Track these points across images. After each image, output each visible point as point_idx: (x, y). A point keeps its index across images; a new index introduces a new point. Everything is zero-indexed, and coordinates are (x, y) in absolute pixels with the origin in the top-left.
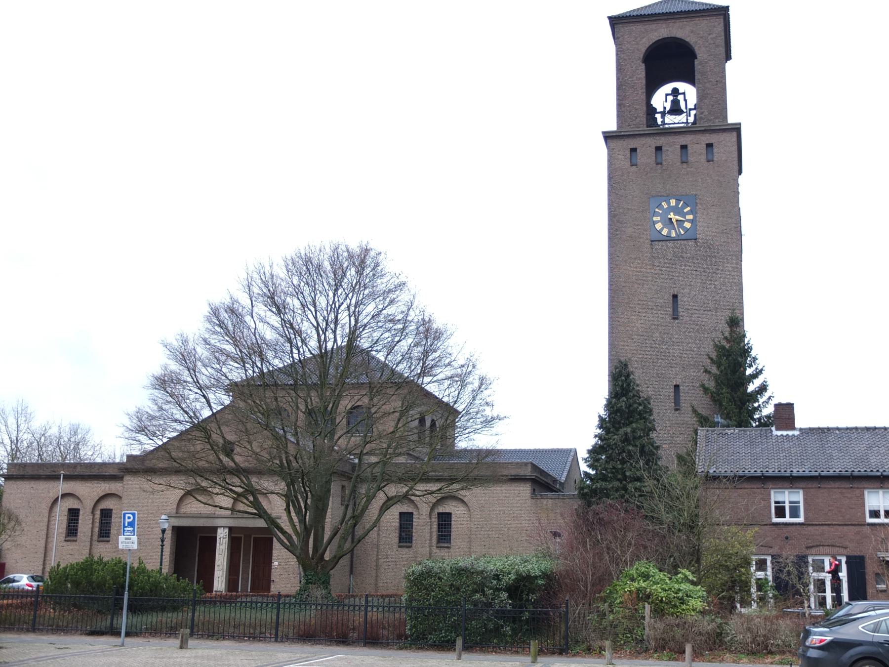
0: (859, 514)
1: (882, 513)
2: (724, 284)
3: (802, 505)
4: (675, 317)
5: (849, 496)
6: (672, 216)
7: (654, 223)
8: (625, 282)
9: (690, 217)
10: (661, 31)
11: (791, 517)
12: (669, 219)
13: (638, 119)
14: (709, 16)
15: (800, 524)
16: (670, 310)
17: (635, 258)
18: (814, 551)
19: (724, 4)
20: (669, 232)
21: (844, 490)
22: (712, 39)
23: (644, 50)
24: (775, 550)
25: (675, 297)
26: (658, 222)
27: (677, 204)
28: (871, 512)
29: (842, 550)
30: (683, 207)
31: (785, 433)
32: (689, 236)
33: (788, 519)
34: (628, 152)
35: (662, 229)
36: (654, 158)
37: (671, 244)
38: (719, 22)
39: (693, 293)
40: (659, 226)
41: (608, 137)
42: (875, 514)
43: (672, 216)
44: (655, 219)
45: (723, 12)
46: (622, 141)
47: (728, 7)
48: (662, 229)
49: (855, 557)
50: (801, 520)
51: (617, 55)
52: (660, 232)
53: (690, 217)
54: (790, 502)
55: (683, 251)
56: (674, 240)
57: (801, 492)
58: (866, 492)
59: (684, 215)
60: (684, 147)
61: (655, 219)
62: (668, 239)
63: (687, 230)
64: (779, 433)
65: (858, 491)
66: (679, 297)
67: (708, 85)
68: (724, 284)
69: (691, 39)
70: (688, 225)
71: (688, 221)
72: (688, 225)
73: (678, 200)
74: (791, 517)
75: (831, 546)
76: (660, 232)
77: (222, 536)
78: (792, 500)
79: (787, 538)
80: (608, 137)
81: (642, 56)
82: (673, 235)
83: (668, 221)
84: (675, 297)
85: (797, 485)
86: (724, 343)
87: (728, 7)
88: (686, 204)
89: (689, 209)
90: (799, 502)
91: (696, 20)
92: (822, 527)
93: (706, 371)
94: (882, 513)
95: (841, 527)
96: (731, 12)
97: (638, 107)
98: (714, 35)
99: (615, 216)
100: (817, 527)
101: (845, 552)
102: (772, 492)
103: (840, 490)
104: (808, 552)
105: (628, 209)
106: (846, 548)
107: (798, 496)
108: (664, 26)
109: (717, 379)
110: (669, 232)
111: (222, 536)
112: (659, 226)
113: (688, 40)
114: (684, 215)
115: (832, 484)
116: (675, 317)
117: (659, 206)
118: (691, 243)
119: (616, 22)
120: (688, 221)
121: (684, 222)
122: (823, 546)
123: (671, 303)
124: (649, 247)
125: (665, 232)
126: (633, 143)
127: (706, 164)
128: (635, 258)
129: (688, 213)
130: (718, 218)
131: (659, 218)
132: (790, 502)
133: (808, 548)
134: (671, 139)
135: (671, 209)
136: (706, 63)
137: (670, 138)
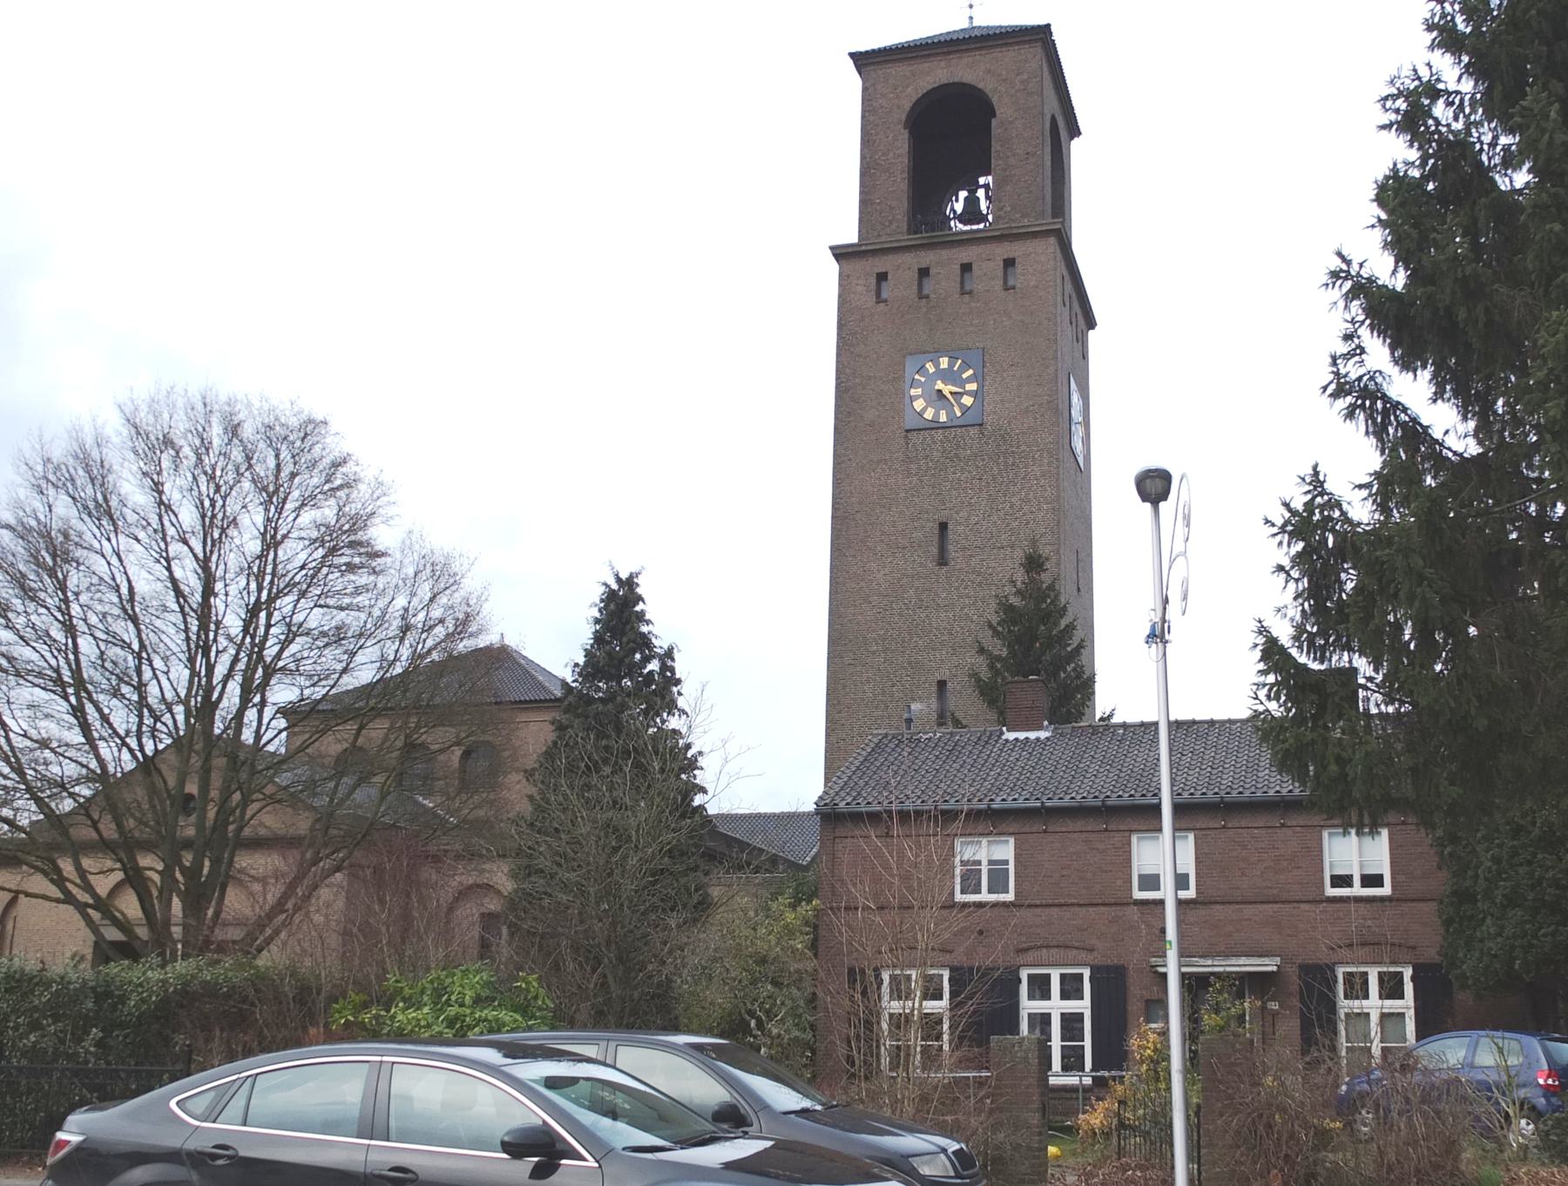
0: (1119, 882)
1: (1357, 881)
2: (1026, 501)
3: (1011, 867)
4: (942, 561)
5: (1101, 846)
6: (940, 385)
7: (912, 399)
8: (860, 503)
9: (972, 387)
10: (939, 73)
11: (990, 891)
12: (936, 392)
13: (894, 226)
14: (1017, 43)
15: (1382, 899)
16: (935, 550)
17: (879, 462)
18: (1030, 956)
19: (1042, 22)
20: (937, 414)
21: (1092, 836)
22: (1022, 82)
23: (907, 106)
24: (959, 958)
25: (943, 527)
26: (918, 397)
27: (951, 365)
28: (1333, 877)
29: (1083, 955)
30: (962, 370)
31: (1022, 735)
32: (969, 420)
33: (985, 896)
34: (873, 281)
35: (924, 409)
36: (915, 287)
37: (939, 435)
38: (1032, 55)
39: (974, 519)
40: (919, 405)
41: (841, 254)
42: (1342, 881)
43: (940, 385)
44: (913, 392)
45: (1041, 36)
46: (863, 262)
47: (1048, 26)
48: (924, 409)
49: (1108, 967)
50: (1010, 897)
51: (863, 117)
52: (920, 414)
53: (972, 387)
54: (991, 862)
55: (958, 446)
56: (944, 427)
57: (1012, 840)
58: (1134, 838)
59: (962, 383)
60: (966, 268)
61: (913, 392)
62: (935, 426)
63: (966, 410)
64: (1011, 736)
65: (1117, 838)
66: (950, 527)
67: (1012, 161)
68: (1026, 501)
69: (987, 85)
70: (967, 401)
71: (968, 393)
72: (967, 401)
73: (953, 359)
74: (990, 891)
75: (1062, 948)
76: (920, 414)
77: (984, 869)
78: (995, 857)
79: (981, 933)
80: (841, 254)
81: (904, 117)
82: (943, 418)
83: (934, 397)
84: (943, 527)
85: (1003, 827)
86: (1015, 601)
87: (1048, 26)
88: (967, 365)
89: (971, 372)
90: (1006, 862)
91: (996, 53)
92: (1047, 910)
93: (982, 651)
94: (1357, 881)
95: (1084, 909)
96: (1058, 36)
97: (895, 204)
98: (1025, 76)
99: (847, 390)
100: (1039, 910)
101: (1089, 958)
102: (958, 843)
103: (1083, 836)
104: (1020, 960)
105: (870, 378)
106: (1092, 950)
107: (1006, 851)
108: (943, 64)
109: (993, 660)
110: (937, 414)
111: (984, 869)
112: (919, 405)
113: (981, 86)
114: (962, 383)
115: (1071, 825)
116: (942, 561)
117: (921, 369)
118: (973, 431)
119: (862, 60)
120: (968, 393)
121: (961, 394)
122: (1047, 947)
123: (936, 539)
124: (902, 441)
125: (929, 415)
126: (880, 264)
127: (1003, 294)
128: (879, 462)
129: (969, 380)
130: (1020, 385)
131: (919, 391)
132: (991, 862)
133: (1020, 951)
134: (945, 254)
135: (947, 376)
136: (1011, 123)
137: (944, 252)
